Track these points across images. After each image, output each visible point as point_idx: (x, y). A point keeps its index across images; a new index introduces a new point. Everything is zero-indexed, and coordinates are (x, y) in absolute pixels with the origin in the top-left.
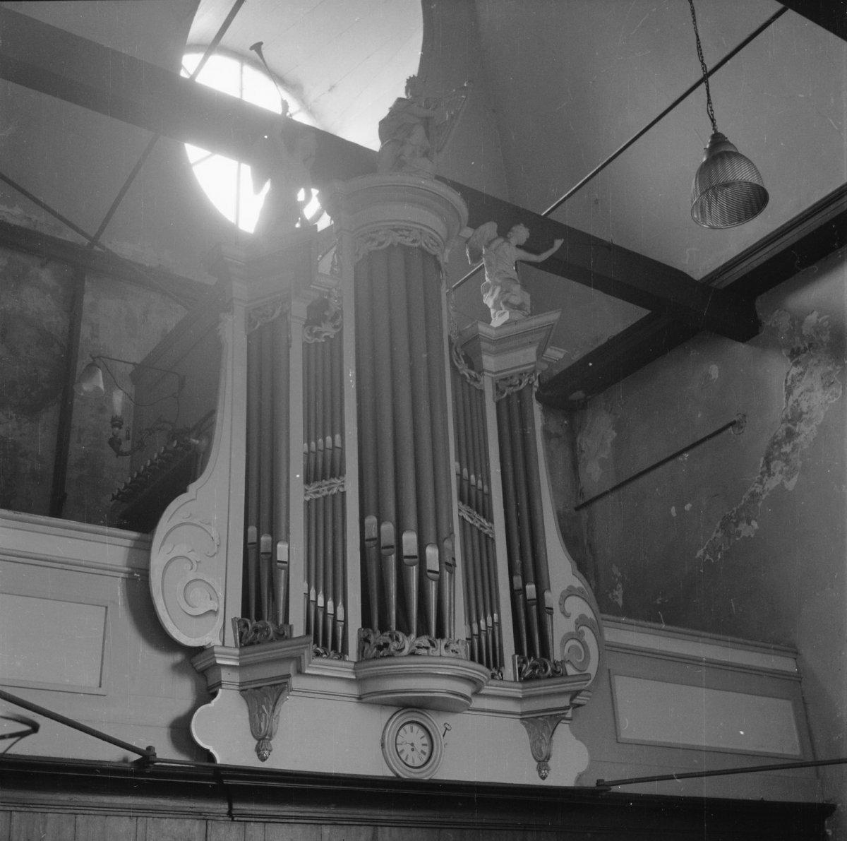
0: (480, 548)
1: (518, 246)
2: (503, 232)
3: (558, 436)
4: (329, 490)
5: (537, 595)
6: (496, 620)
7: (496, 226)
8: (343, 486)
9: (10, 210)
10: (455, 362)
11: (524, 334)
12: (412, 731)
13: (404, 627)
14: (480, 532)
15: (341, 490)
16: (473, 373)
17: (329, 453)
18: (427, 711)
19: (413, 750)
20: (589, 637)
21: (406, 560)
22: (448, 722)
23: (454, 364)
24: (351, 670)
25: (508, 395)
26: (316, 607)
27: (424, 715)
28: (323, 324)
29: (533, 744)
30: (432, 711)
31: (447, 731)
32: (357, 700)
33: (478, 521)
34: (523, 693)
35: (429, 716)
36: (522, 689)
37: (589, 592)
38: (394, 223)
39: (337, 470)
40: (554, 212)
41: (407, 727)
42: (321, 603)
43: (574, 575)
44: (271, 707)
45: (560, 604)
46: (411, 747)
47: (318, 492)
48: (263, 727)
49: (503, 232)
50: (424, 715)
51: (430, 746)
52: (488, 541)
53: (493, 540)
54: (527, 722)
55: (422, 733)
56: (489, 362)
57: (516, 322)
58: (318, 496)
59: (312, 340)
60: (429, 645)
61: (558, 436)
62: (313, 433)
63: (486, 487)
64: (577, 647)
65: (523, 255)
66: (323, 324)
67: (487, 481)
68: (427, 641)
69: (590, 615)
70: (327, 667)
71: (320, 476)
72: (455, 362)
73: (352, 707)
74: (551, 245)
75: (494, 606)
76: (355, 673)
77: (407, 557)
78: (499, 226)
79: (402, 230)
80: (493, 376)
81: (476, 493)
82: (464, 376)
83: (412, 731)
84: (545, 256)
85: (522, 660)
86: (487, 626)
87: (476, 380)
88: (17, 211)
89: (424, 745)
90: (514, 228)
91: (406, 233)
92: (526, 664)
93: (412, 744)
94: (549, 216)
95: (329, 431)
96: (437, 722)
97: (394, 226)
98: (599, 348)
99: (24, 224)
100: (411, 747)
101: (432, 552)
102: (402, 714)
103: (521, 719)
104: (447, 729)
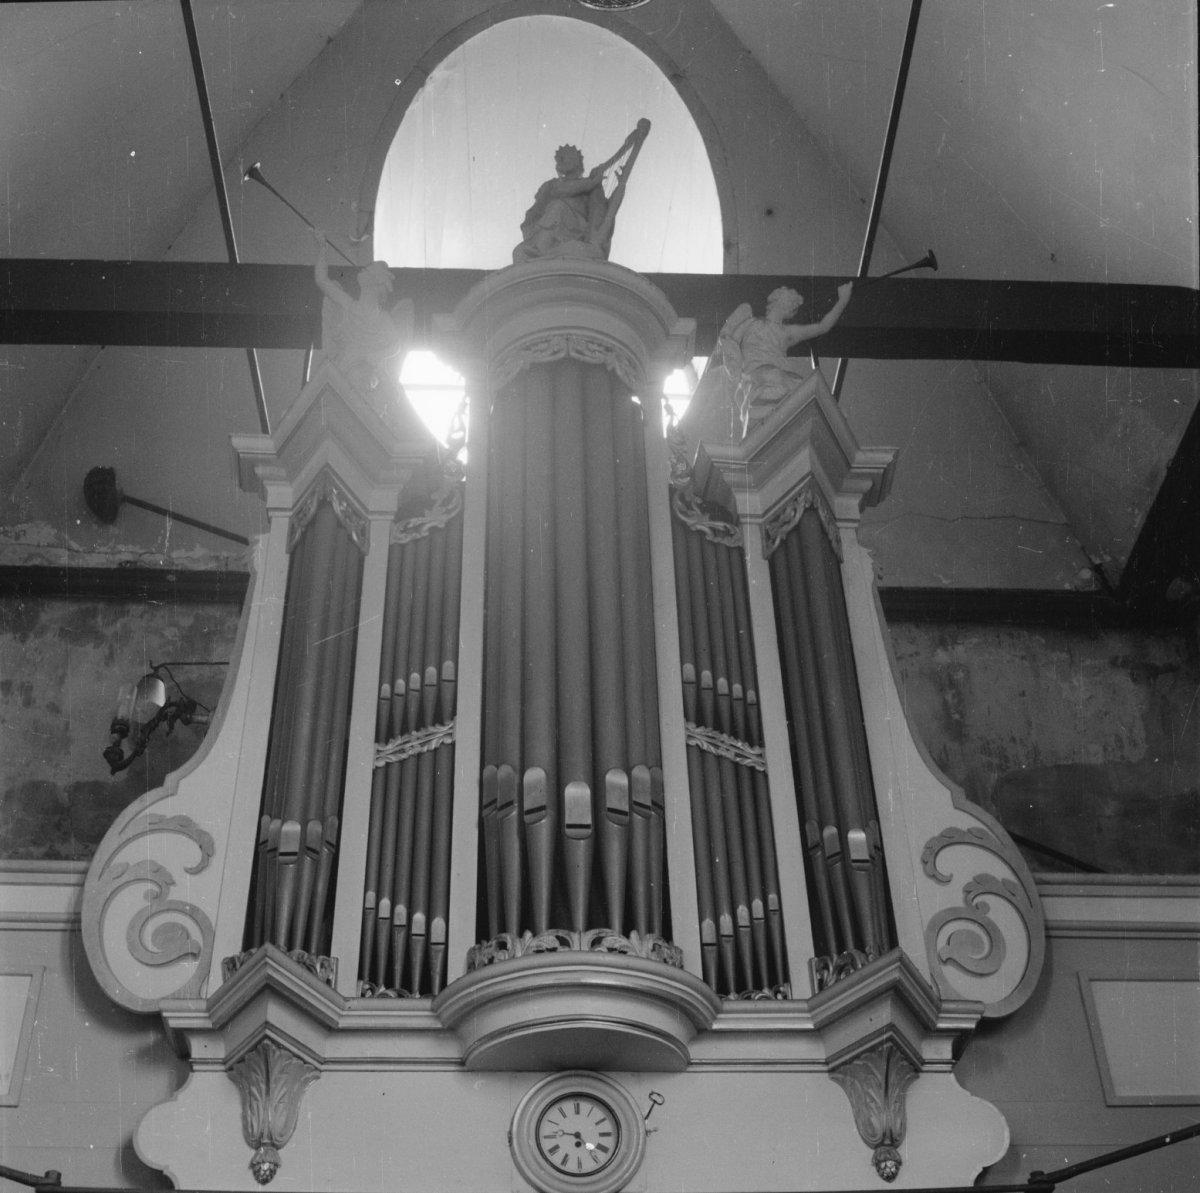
0: (739, 797)
1: (788, 321)
2: (760, 312)
3: (1171, 669)
4: (422, 745)
5: (842, 848)
6: (773, 906)
7: (749, 306)
8: (451, 735)
9: (190, 554)
10: (680, 516)
11: (783, 432)
12: (578, 1112)
13: (527, 923)
14: (736, 765)
15: (448, 741)
16: (720, 525)
17: (431, 694)
18: (611, 1074)
19: (578, 1145)
20: (1002, 914)
21: (569, 831)
22: (656, 1091)
23: (679, 519)
24: (426, 1013)
25: (782, 540)
26: (392, 927)
27: (614, 1087)
28: (427, 512)
29: (857, 1115)
30: (623, 1074)
31: (656, 1106)
32: (457, 1068)
33: (730, 747)
34: (812, 1018)
35: (618, 1087)
36: (809, 1011)
37: (999, 833)
38: (524, 340)
39: (448, 708)
40: (873, 263)
41: (568, 1106)
42: (401, 917)
43: (956, 808)
44: (263, 1086)
45: (925, 862)
46: (575, 1140)
47: (403, 751)
48: (255, 1125)
49: (760, 312)
50: (614, 1087)
51: (616, 1135)
52: (755, 781)
53: (765, 775)
54: (840, 1076)
55: (598, 1113)
56: (749, 503)
57: (762, 421)
58: (404, 756)
59: (406, 539)
60: (556, 944)
61: (1171, 669)
62: (402, 663)
63: (751, 695)
64: (970, 933)
65: (799, 332)
66: (427, 512)
67: (750, 679)
68: (552, 938)
69: (1000, 871)
70: (315, 993)
71: (412, 724)
72: (680, 516)
73: (449, 1081)
74: (836, 298)
75: (767, 880)
76: (438, 1017)
77: (571, 826)
78: (751, 304)
79: (536, 344)
80: (760, 521)
81: (731, 707)
82: (701, 533)
83: (578, 1112)
84: (830, 319)
85: (822, 965)
86: (751, 918)
87: (727, 533)
88: (199, 552)
89: (603, 1135)
90: (770, 298)
91: (543, 346)
92: (828, 969)
93: (577, 1135)
94: (871, 273)
95: (432, 655)
96: (632, 1092)
97: (525, 343)
98: (1163, 488)
99: (212, 566)
100: (575, 1140)
101: (577, 793)
102: (556, 1080)
103: (829, 1071)
104: (655, 1102)
